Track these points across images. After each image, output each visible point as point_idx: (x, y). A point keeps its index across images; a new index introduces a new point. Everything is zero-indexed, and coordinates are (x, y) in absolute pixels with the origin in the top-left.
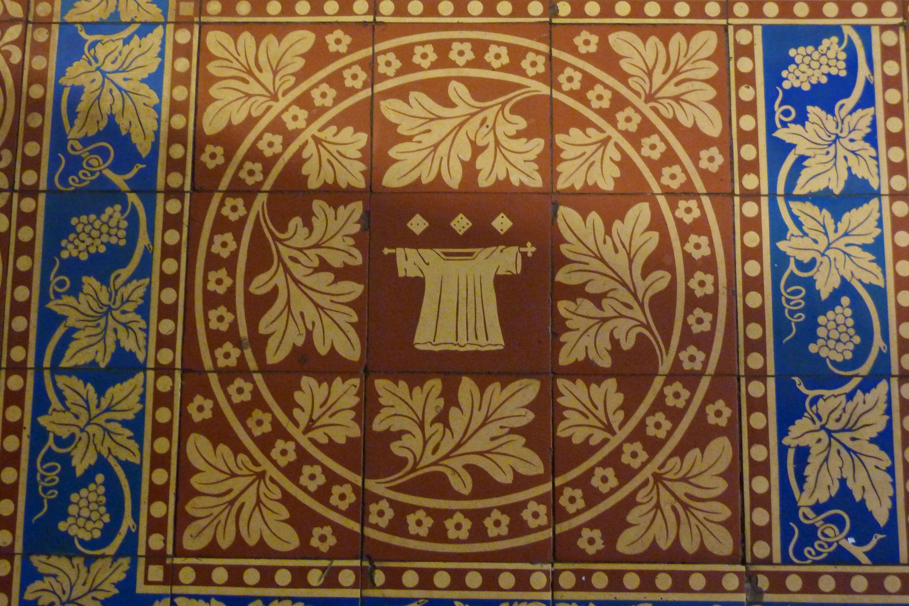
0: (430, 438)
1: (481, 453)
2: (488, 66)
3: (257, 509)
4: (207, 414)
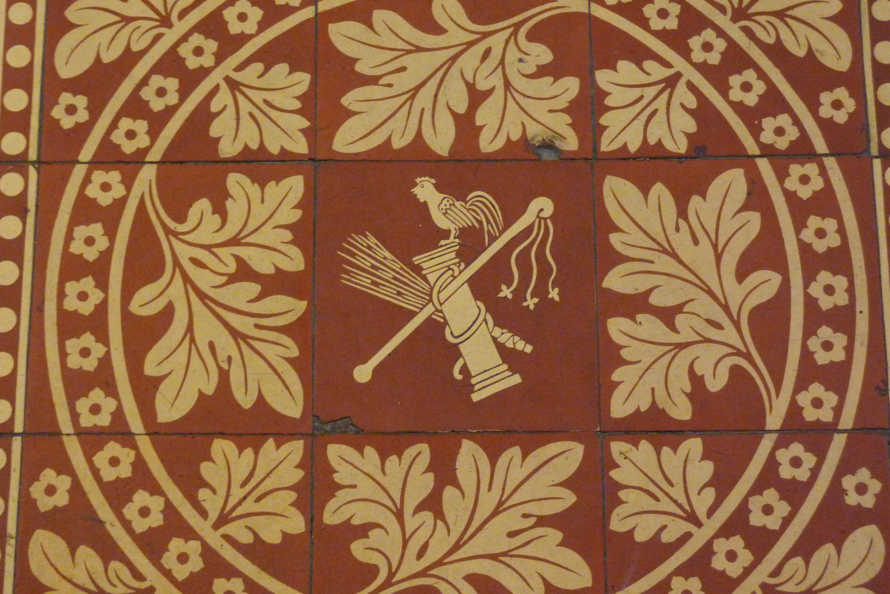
1: (190, 329)
2: (106, 256)
3: (117, 19)
4: (61, 499)
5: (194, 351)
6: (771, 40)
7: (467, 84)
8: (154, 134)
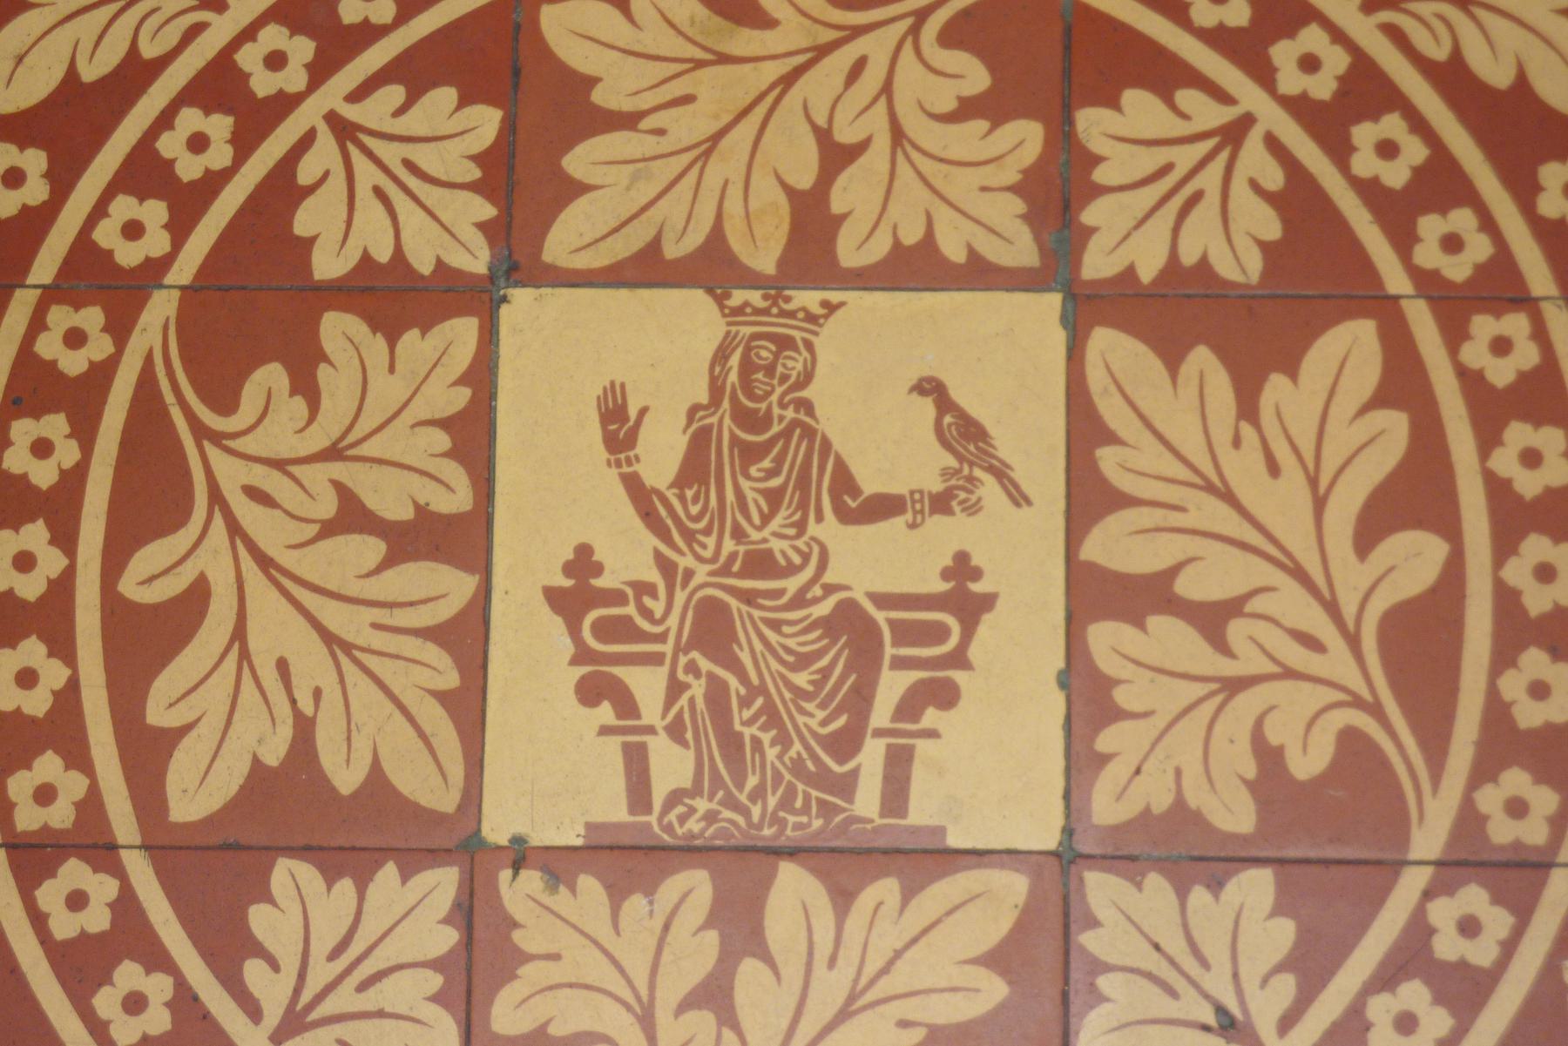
0: (875, 100)
5: (246, 671)
6: (1439, 52)
7: (816, 129)
8: (1419, 931)
